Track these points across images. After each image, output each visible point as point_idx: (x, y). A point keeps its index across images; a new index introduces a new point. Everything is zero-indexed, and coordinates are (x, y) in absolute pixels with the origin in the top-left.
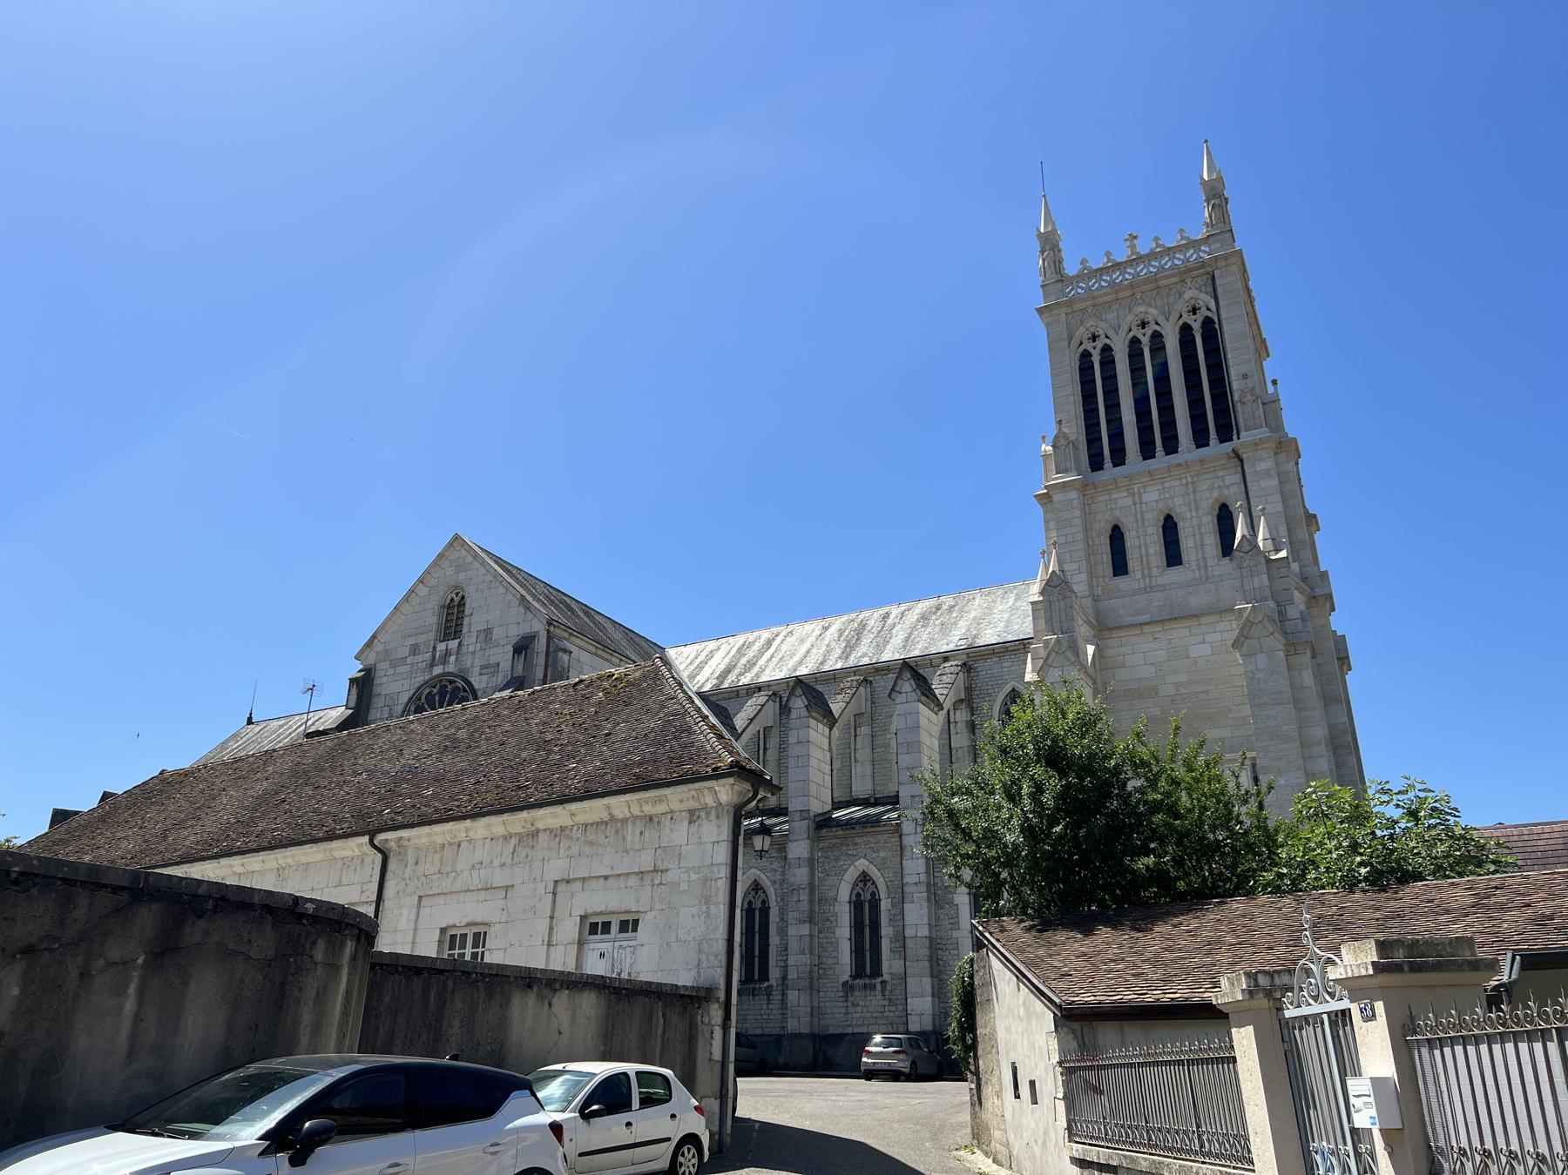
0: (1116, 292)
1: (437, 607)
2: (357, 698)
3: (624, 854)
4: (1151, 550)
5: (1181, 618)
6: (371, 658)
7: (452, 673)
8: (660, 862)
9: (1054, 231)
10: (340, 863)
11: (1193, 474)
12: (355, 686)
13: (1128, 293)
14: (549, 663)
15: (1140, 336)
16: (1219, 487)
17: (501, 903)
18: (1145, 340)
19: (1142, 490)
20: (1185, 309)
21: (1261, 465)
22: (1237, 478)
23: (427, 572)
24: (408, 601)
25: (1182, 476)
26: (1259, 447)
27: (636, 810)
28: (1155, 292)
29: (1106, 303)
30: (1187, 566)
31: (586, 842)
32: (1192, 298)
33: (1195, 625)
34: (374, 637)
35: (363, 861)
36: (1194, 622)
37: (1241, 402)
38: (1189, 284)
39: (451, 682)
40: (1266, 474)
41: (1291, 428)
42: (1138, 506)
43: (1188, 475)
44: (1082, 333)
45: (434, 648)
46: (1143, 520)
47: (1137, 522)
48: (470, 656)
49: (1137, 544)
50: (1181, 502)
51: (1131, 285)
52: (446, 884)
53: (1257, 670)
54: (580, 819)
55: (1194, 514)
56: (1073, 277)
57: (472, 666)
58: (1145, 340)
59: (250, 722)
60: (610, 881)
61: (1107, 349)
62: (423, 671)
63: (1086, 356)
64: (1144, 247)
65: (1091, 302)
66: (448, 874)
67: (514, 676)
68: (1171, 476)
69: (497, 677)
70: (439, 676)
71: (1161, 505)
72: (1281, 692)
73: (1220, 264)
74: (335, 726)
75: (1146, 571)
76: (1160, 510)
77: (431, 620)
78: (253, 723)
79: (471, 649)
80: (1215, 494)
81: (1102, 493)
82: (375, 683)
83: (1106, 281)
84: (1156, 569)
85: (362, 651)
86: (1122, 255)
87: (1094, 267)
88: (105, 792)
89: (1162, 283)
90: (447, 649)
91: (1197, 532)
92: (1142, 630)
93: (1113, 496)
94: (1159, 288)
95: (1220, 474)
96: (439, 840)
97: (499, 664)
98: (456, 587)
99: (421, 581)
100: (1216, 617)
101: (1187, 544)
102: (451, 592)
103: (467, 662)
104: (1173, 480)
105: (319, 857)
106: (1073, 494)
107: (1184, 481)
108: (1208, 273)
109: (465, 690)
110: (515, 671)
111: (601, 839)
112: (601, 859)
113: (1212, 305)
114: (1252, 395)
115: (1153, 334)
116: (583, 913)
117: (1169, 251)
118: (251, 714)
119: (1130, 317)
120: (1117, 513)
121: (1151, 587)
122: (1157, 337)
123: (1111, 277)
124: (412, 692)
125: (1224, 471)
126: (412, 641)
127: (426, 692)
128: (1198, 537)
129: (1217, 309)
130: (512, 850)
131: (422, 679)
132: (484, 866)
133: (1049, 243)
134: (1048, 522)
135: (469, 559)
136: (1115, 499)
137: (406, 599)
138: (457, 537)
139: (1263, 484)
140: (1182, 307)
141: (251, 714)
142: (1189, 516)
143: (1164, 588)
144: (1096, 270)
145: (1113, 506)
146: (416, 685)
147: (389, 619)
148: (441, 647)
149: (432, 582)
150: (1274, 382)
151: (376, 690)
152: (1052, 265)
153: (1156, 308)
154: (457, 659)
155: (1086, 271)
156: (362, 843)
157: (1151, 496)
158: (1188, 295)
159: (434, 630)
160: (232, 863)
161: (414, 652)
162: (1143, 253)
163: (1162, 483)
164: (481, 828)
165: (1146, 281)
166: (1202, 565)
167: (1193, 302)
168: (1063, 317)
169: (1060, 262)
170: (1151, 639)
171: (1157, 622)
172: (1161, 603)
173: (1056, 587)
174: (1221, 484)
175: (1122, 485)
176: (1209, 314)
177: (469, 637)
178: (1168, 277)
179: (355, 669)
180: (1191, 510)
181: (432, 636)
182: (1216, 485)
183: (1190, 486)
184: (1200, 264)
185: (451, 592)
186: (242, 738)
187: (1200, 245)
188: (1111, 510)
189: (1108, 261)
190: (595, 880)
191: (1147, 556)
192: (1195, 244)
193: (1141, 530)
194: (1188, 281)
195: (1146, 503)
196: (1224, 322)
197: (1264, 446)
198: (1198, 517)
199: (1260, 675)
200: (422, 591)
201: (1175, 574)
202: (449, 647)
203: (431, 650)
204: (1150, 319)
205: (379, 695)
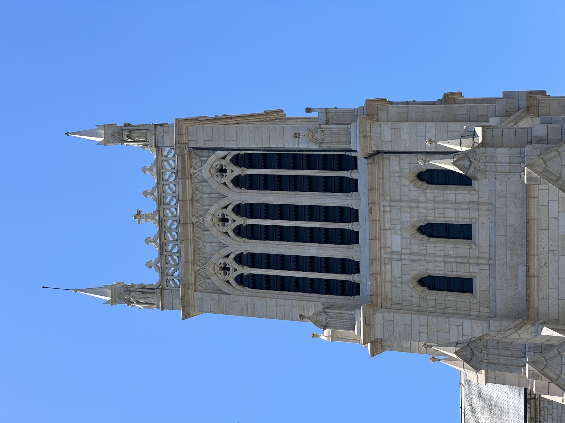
4: (451, 252)
9: (112, 287)
13: (190, 228)
15: (235, 225)
16: (400, 176)
18: (238, 171)
22: (394, 159)
25: (382, 209)
28: (196, 204)
29: (194, 251)
30: (474, 220)
32: (210, 171)
38: (195, 171)
42: (403, 257)
43: (382, 204)
44: (218, 280)
46: (419, 254)
49: (443, 264)
50: (408, 215)
55: (422, 205)
56: (162, 278)
58: (238, 171)
63: (241, 280)
64: (150, 206)
65: (190, 265)
68: (380, 221)
71: (407, 235)
73: (185, 139)
75: (472, 261)
81: (383, 288)
83: (173, 248)
84: (471, 251)
86: (153, 228)
89: (189, 196)
93: (389, 278)
94: (192, 200)
95: (387, 174)
100: (533, 202)
106: (378, 317)
107: (388, 209)
108: (190, 152)
113: (221, 153)
117: (160, 184)
120: (407, 278)
121: (490, 259)
123: (170, 218)
125: (385, 170)
129: (226, 150)
140: (216, 182)
152: (144, 295)
158: (206, 174)
163: (385, 229)
167: (213, 171)
170: (545, 269)
172: (508, 252)
174: (397, 175)
176: (229, 158)
182: (398, 180)
183: (393, 204)
184: (179, 158)
192: (160, 160)
197: (368, 130)
198: (426, 201)
201: (480, 233)
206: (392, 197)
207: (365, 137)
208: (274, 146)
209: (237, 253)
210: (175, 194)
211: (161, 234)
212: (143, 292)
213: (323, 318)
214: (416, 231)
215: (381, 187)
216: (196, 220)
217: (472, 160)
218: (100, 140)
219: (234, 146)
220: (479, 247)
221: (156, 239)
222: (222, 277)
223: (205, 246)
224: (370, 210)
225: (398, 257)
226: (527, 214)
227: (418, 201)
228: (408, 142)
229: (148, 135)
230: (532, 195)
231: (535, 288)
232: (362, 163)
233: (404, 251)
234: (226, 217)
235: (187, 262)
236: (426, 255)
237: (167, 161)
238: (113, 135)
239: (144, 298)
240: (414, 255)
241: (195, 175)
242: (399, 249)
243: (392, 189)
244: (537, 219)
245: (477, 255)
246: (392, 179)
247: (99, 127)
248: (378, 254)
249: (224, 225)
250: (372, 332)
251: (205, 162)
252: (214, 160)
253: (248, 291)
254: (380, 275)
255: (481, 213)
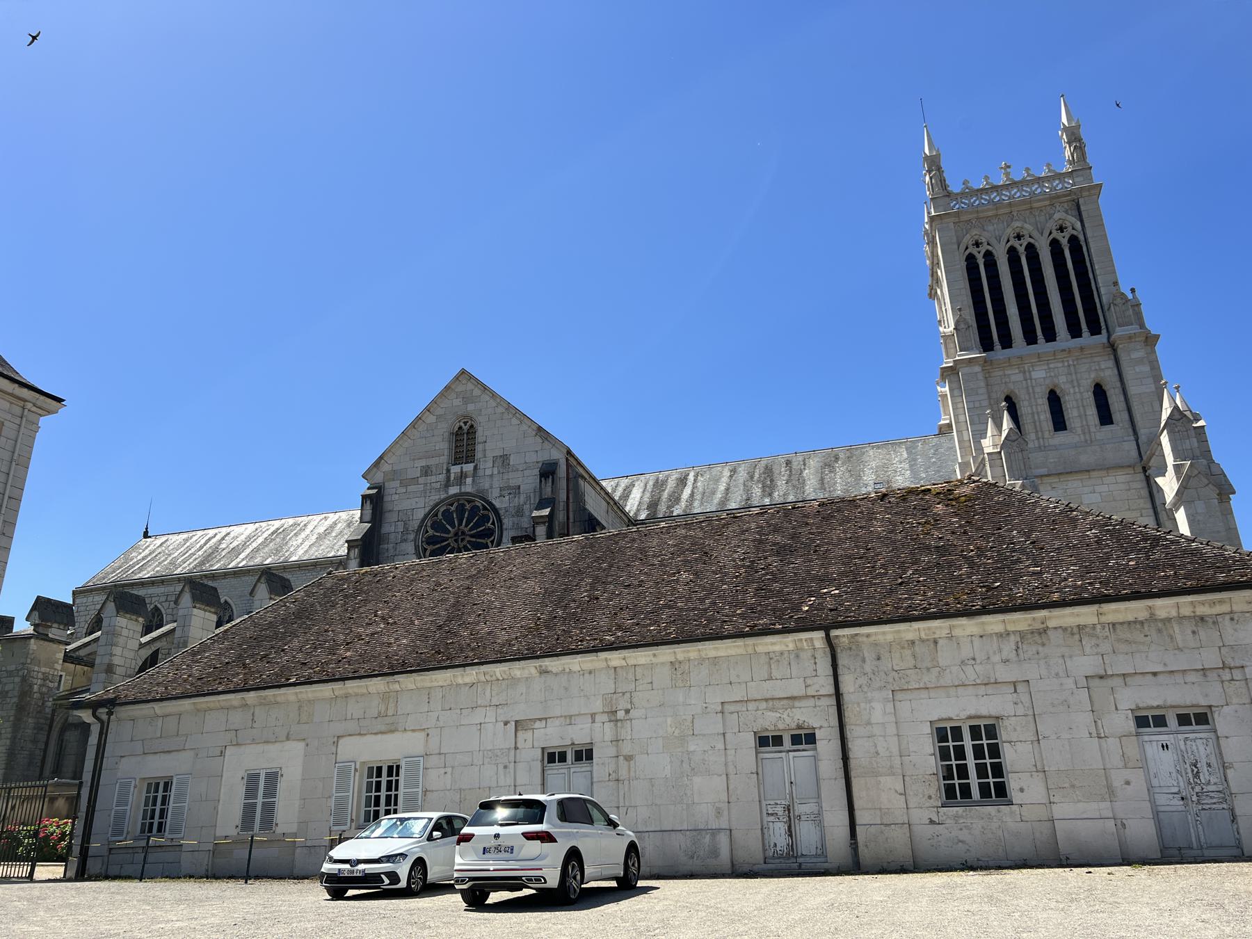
0: (997, 209)
1: (447, 433)
2: (372, 513)
3: (1176, 652)
4: (1042, 417)
5: (1076, 472)
6: (378, 478)
7: (468, 493)
8: (1230, 660)
9: (938, 156)
10: (764, 659)
11: (1074, 358)
12: (368, 502)
13: (1007, 210)
14: (570, 488)
15: (975, 253)
16: (1096, 370)
17: (1011, 698)
18: (1064, 242)
19: (1031, 369)
20: (1054, 228)
21: (1132, 355)
22: (1111, 363)
23: (434, 401)
24: (414, 427)
25: (1065, 359)
26: (1133, 340)
27: (1187, 611)
28: (1028, 212)
29: (988, 217)
31: (1119, 640)
32: (1060, 219)
33: (1086, 479)
34: (381, 458)
35: (797, 656)
36: (1085, 476)
37: (1113, 303)
38: (1057, 207)
39: (469, 502)
40: (1140, 361)
41: (1152, 326)
42: (1029, 381)
43: (1070, 359)
44: (968, 240)
45: (448, 471)
46: (1034, 392)
47: (1029, 394)
48: (487, 479)
49: (1030, 412)
50: (1065, 380)
51: (1010, 204)
52: (929, 679)
53: (1197, 513)
54: (1110, 618)
55: (1077, 390)
56: (957, 194)
57: (491, 487)
58: (1064, 242)
59: (146, 535)
60: (1160, 678)
61: (988, 255)
62: (438, 490)
63: (971, 259)
64: (1019, 174)
65: (975, 215)
66: (928, 669)
67: (544, 497)
68: (1055, 359)
69: (519, 498)
70: (455, 495)
71: (1048, 382)
72: (1218, 532)
73: (1085, 194)
74: (359, 537)
75: (1040, 434)
76: (1047, 385)
77: (442, 446)
78: (150, 537)
79: (488, 472)
80: (1093, 375)
82: (384, 500)
83: (986, 200)
84: (1048, 432)
85: (369, 470)
86: (1002, 180)
87: (976, 188)
88: (38, 597)
89: (1035, 205)
90: (462, 472)
91: (1080, 404)
92: (1089, 475)
93: (1007, 372)
94: (1031, 208)
95: (1096, 359)
96: (910, 636)
97: (519, 487)
98: (465, 417)
99: (428, 409)
100: (1103, 473)
101: (1071, 412)
102: (459, 421)
103: (485, 484)
104: (1057, 362)
105: (741, 651)
106: (977, 369)
107: (1066, 364)
108: (1073, 201)
109: (485, 508)
110: (543, 493)
111: (1141, 638)
112: (1147, 657)
113: (1078, 225)
114: (1122, 298)
115: (1070, 237)
116: (1133, 707)
117: (1039, 180)
118: (147, 529)
119: (1009, 231)
120: (1011, 386)
121: (1045, 447)
122: (1031, 249)
123: (990, 197)
124: (427, 510)
125: (1099, 358)
126: (423, 463)
127: (442, 510)
128: (1080, 408)
129: (1083, 230)
130: (1014, 647)
131: (437, 497)
132: (978, 661)
133: (934, 164)
134: (953, 390)
135: (477, 392)
136: (1009, 375)
137: (413, 425)
138: (463, 372)
139: (1137, 369)
140: (1052, 225)
141: (147, 529)
142: (1072, 391)
143: (1056, 448)
144: (978, 190)
145: (1008, 380)
146: (432, 503)
147: (396, 442)
148: (455, 469)
149: (439, 411)
150: (1133, 290)
151: (387, 506)
152: (939, 183)
153: (1030, 224)
154: (473, 481)
155: (967, 190)
156: (801, 640)
157: (1039, 374)
158: (1057, 216)
159: (446, 454)
160: (609, 657)
161: (426, 472)
162: (1016, 179)
163: (1048, 364)
164: (966, 627)
165: (1023, 202)
166: (1086, 431)
167: (1060, 222)
168: (952, 225)
169: (945, 181)
170: (1050, 488)
171: (1056, 474)
172: (1056, 460)
173: (1014, 441)
174: (1097, 368)
175: (1015, 363)
176: (1075, 233)
177: (485, 461)
178: (1040, 201)
179: (363, 487)
180: (1074, 387)
181: (444, 459)
182: (1093, 368)
183: (1072, 368)
184: (1067, 192)
185: (459, 421)
186: (144, 551)
187: (1064, 178)
188: (1006, 383)
189: (987, 184)
190: (1140, 676)
191: (1040, 422)
192: (1060, 176)
193: (1033, 400)
194: (1057, 205)
195: (1035, 379)
196: (1090, 240)
197: (1137, 339)
198: (1081, 393)
199: (1199, 518)
200: (431, 419)
201: (1061, 437)
202: (464, 470)
203: (444, 472)
204: (1025, 232)
205: (390, 511)
206: (1077, 366)
207: (1130, 338)
208: (1096, 267)
209: (994, 251)
210: (1032, 193)
211: (995, 188)
212: (941, 181)
213: (962, 326)
214: (1051, 387)
215: (1083, 356)
216: (1015, 215)
217: (1181, 421)
218: (927, 151)
219: (1089, 234)
220: (1052, 438)
221: (969, 189)
222: (970, 243)
223: (993, 225)
224: (1064, 350)
225: (1028, 377)
226: (1094, 470)
227: (1079, 386)
228: (1134, 372)
229: (1081, 163)
230: (1109, 471)
231: (1069, 479)
232: (1102, 338)
233: (1033, 381)
234: (1065, 230)
235: (977, 212)
236: (1035, 398)
237: (998, 195)
238: (1073, 134)
239: (937, 182)
240: (1033, 389)
241: (1054, 208)
242: (1034, 377)
243: (1083, 365)
244: (1090, 478)
245: (1045, 437)
246: (1093, 364)
247: (938, 151)
248: (1026, 362)
249: (973, 245)
250: (964, 365)
251: (1068, 214)
252: (1071, 221)
253: (964, 264)
254: (1009, 366)
255: (1082, 436)
